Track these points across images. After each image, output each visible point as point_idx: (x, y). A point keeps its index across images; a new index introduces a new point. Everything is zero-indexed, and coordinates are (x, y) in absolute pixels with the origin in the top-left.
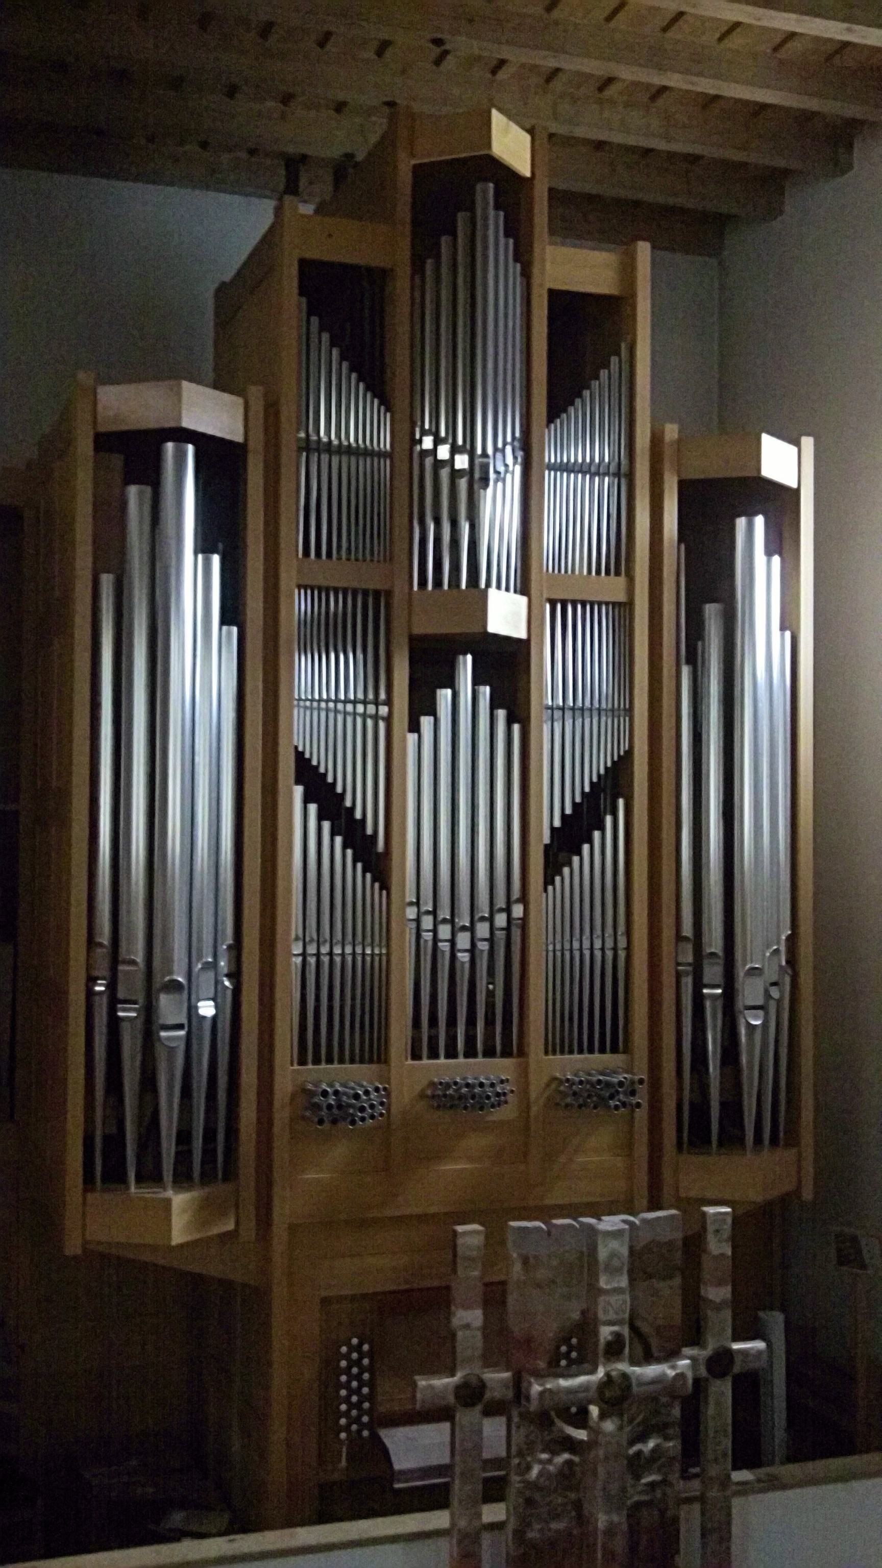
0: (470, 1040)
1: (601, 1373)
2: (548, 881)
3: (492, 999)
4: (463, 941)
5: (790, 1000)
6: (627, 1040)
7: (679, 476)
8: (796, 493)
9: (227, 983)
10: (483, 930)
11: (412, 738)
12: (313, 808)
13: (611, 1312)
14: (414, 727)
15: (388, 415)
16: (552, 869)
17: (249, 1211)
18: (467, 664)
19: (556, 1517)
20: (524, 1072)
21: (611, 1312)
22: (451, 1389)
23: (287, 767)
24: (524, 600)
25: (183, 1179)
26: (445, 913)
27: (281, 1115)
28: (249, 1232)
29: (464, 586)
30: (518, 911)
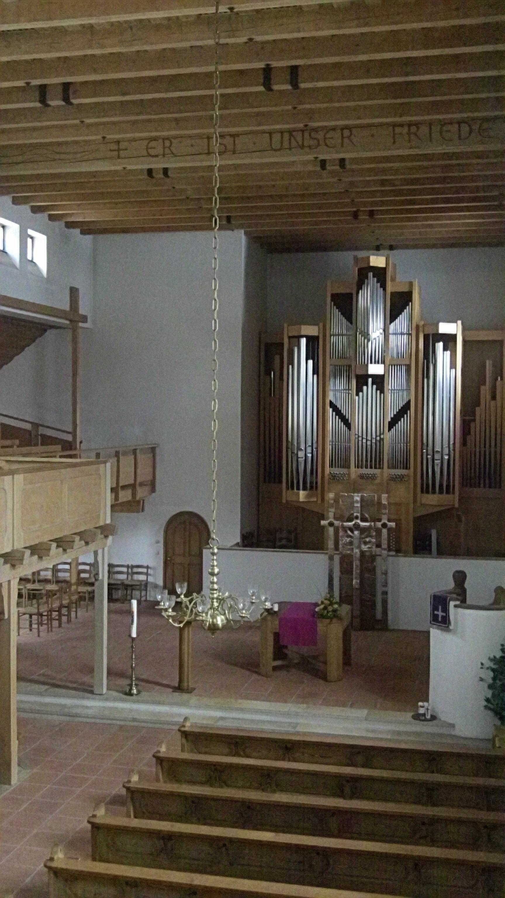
0: (362, 464)
1: (353, 523)
2: (389, 430)
6: (380, 465)
10: (374, 441)
11: (357, 398)
12: (334, 413)
14: (357, 395)
15: (310, 362)
17: (319, 496)
18: (370, 380)
24: (383, 365)
25: (305, 489)
26: (364, 436)
28: (319, 501)
30: (382, 436)
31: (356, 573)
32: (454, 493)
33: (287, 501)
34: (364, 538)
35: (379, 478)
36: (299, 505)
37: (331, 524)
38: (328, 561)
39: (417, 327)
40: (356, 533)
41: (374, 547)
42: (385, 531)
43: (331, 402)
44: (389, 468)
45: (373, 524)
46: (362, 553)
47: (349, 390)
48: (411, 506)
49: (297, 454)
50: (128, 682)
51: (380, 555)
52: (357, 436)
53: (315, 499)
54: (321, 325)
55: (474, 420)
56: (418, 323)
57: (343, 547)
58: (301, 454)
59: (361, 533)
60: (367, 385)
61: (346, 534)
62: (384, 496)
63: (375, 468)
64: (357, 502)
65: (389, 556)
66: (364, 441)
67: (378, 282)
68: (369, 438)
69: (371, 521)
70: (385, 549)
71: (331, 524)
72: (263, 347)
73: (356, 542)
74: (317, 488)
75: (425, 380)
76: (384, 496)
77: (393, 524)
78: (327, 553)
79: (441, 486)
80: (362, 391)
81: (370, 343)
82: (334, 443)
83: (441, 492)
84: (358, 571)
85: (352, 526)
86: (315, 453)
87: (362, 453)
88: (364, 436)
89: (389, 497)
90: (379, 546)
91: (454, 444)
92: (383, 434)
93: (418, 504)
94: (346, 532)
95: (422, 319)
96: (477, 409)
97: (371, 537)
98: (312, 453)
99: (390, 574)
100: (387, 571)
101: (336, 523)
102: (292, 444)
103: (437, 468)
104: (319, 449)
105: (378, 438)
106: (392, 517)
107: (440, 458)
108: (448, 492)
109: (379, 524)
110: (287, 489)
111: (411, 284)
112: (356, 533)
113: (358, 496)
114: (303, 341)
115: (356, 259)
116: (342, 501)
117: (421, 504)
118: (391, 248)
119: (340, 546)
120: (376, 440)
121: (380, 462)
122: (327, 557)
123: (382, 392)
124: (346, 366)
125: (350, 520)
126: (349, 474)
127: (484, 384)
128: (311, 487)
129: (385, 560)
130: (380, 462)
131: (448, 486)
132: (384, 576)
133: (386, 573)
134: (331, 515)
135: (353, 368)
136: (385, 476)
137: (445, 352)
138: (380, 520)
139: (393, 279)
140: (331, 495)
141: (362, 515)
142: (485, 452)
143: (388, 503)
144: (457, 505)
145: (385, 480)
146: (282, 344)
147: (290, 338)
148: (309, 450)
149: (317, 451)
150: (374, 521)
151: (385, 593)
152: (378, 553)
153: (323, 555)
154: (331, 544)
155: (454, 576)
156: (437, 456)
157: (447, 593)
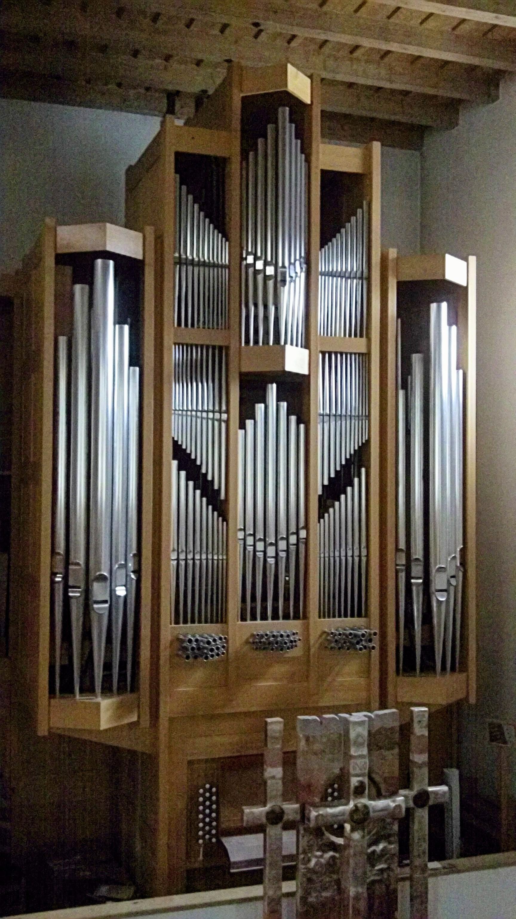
4: (271, 551)
9: (133, 576)
10: (282, 545)
11: (241, 432)
12: (183, 474)
13: (358, 769)
14: (242, 426)
19: (325, 889)
20: (307, 628)
21: (358, 769)
24: (307, 351)
25: (107, 690)
27: (165, 654)
28: (146, 722)
30: (303, 534)
43: (175, 443)
50: (285, 902)
54: (149, 230)
60: (265, 137)
80: (253, 417)
82: (182, 556)
104: (143, 573)
105: (293, 539)
135: (232, 352)
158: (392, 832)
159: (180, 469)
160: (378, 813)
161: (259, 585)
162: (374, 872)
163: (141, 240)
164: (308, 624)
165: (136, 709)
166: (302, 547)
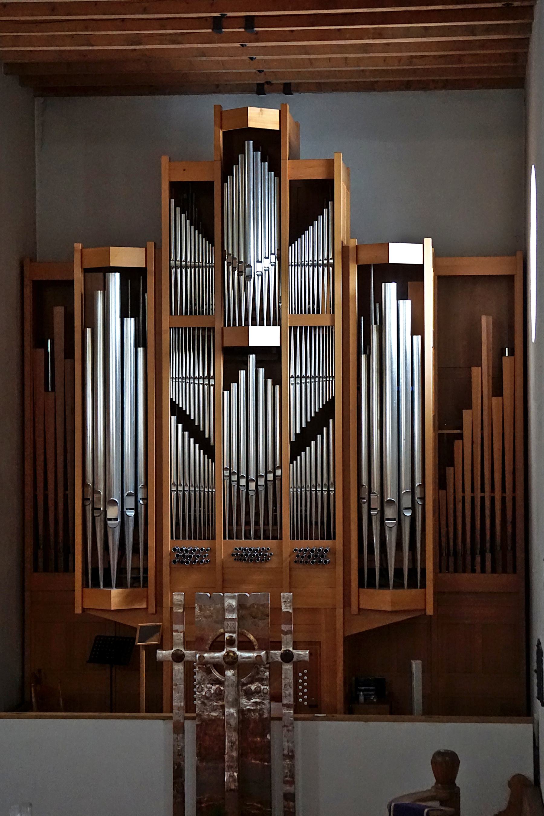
0: (239, 531)
3: (275, 514)
4: (252, 486)
5: (362, 513)
7: (357, 263)
8: (420, 268)
9: (141, 502)
10: (262, 482)
11: (226, 393)
13: (229, 627)
14: (227, 388)
15: (130, 323)
16: (295, 454)
18: (252, 358)
19: (214, 710)
20: (280, 547)
21: (229, 627)
22: (171, 653)
23: (167, 408)
25: (119, 585)
26: (243, 473)
27: (166, 561)
28: (152, 609)
29: (243, 325)
30: (278, 472)
31: (231, 757)
32: (423, 586)
33: (84, 610)
34: (246, 684)
35: (274, 559)
36: (106, 616)
37: (178, 657)
38: (171, 737)
39: (345, 249)
40: (229, 673)
41: (266, 702)
42: (288, 668)
43: (173, 403)
44: (293, 537)
45: (263, 653)
46: (241, 712)
47: (209, 378)
48: (340, 611)
49: (105, 512)
51: (280, 719)
52: (227, 473)
53: (144, 606)
55: (460, 437)
56: (345, 243)
57: (203, 703)
58: (113, 512)
59: (239, 676)
61: (209, 677)
62: (286, 595)
63: (266, 537)
64: (231, 609)
65: (296, 719)
66: (243, 482)
67: (263, 160)
68: (252, 476)
69: (261, 649)
70: (288, 706)
71: (178, 657)
72: (28, 290)
73: (230, 693)
74: (146, 579)
75: (363, 357)
76: (286, 595)
77: (303, 654)
78: (170, 718)
79: (399, 572)
81: (250, 284)
83: (399, 585)
84: (235, 754)
85: (221, 660)
86: (141, 510)
87: (239, 506)
88: (243, 473)
89: (294, 600)
90: (276, 697)
91: (423, 485)
92: (281, 467)
93: (354, 608)
94: (209, 672)
95: (352, 234)
96: (467, 414)
97: (261, 680)
98: (136, 509)
99: (299, 755)
100: (292, 751)
101: (188, 653)
102: (95, 491)
103: (391, 536)
105: (270, 477)
106: (301, 637)
107: (396, 516)
108: (412, 585)
109: (276, 654)
110: (85, 585)
111: (330, 164)
112: (229, 673)
113: (233, 598)
114: (115, 280)
115: (220, 113)
116: (200, 609)
117: (359, 609)
118: (288, 89)
119: (198, 702)
120: (266, 481)
121: (275, 523)
122: (170, 725)
123: (277, 382)
124: (204, 329)
125: (217, 646)
126: (212, 551)
127: (479, 364)
128: (135, 580)
129: (289, 728)
130: (275, 523)
131: (412, 571)
132: (288, 761)
133: (291, 756)
134: (178, 636)
136: (286, 553)
137: (401, 302)
138: (277, 645)
139: (294, 156)
140: (178, 597)
141: (240, 634)
142: (483, 498)
143: (294, 609)
144: (430, 611)
145: (286, 564)
146: (71, 283)
147: (86, 271)
148: (130, 502)
149: (146, 506)
150: (267, 650)
151: (290, 797)
152: (274, 714)
153: (161, 722)
154: (178, 701)
155: (434, 763)
156: (390, 512)
157: (420, 800)
158: (265, 677)
159: (178, 422)
160: (244, 660)
161: (419, 529)
162: (250, 703)
163: (144, 252)
164: (282, 542)
165: (145, 600)
166: (278, 483)
